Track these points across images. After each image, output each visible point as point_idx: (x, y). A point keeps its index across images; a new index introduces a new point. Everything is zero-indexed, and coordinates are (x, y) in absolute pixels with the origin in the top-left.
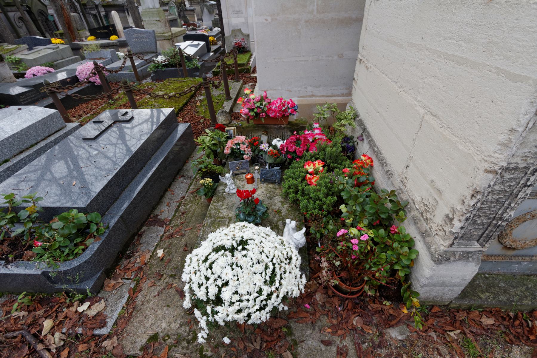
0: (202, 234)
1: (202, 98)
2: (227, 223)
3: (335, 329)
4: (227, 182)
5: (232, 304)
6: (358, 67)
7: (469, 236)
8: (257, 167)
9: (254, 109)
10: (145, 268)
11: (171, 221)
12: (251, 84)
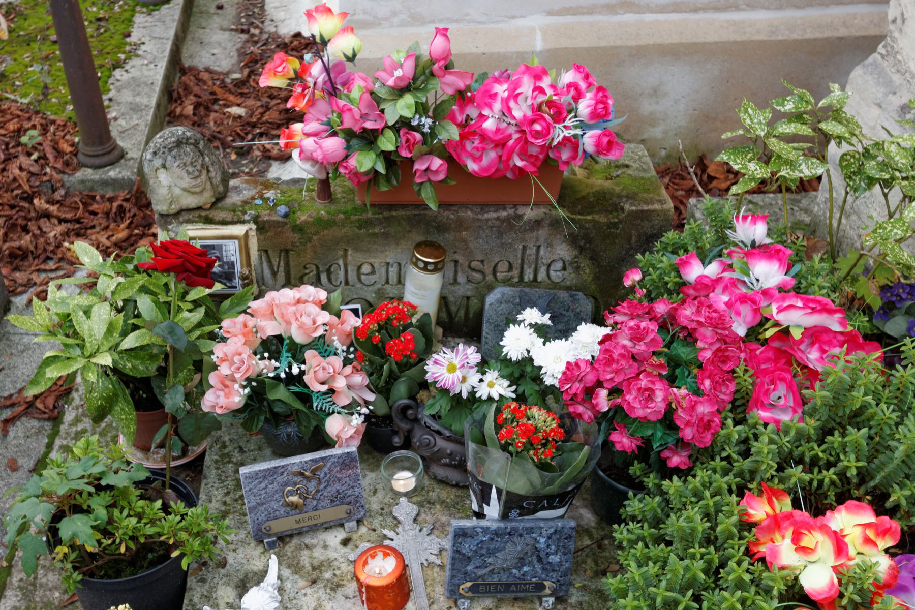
8: (404, 481)
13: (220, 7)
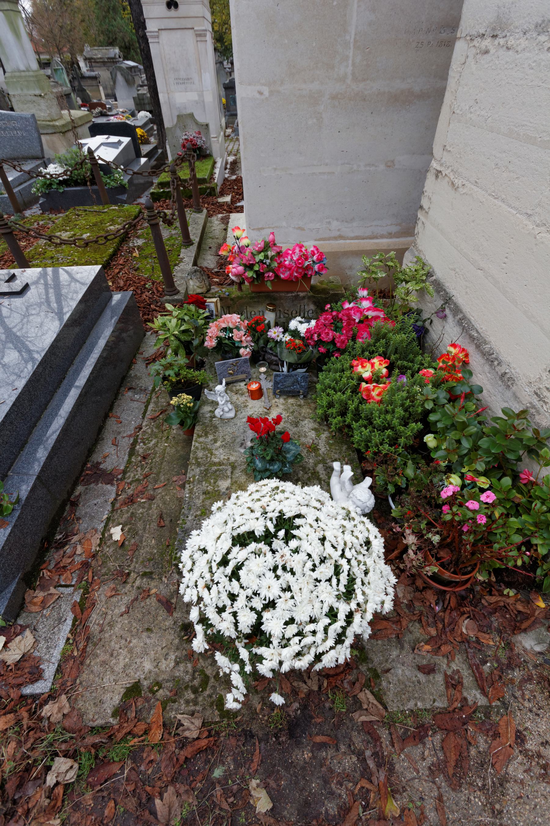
0: (190, 497)
1: (140, 242)
2: (229, 473)
3: (438, 643)
4: (219, 399)
5: (285, 643)
8: (263, 369)
9: (253, 265)
10: (93, 563)
11: (124, 472)
12: (220, 216)
13: (210, 248)
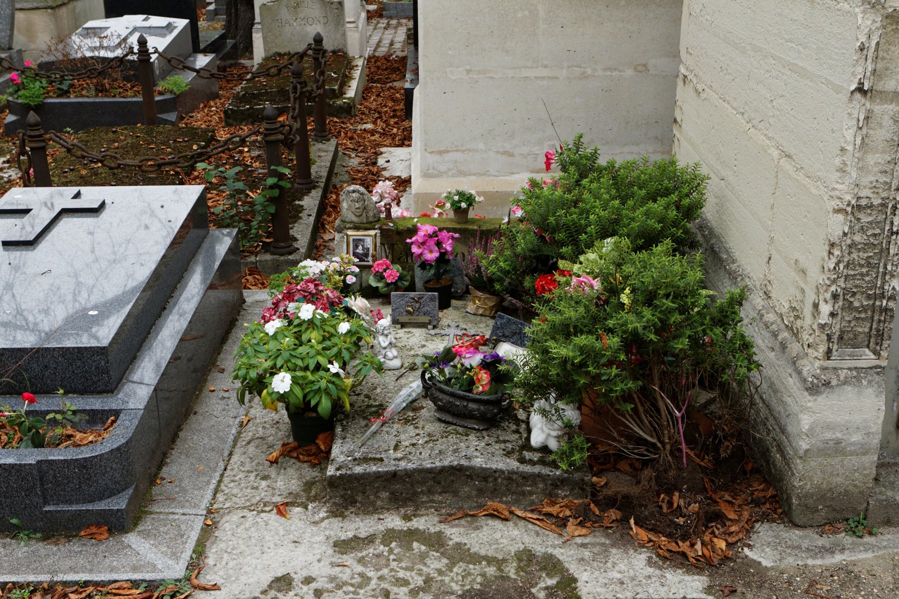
6: (683, 94)
7: (851, 335)
